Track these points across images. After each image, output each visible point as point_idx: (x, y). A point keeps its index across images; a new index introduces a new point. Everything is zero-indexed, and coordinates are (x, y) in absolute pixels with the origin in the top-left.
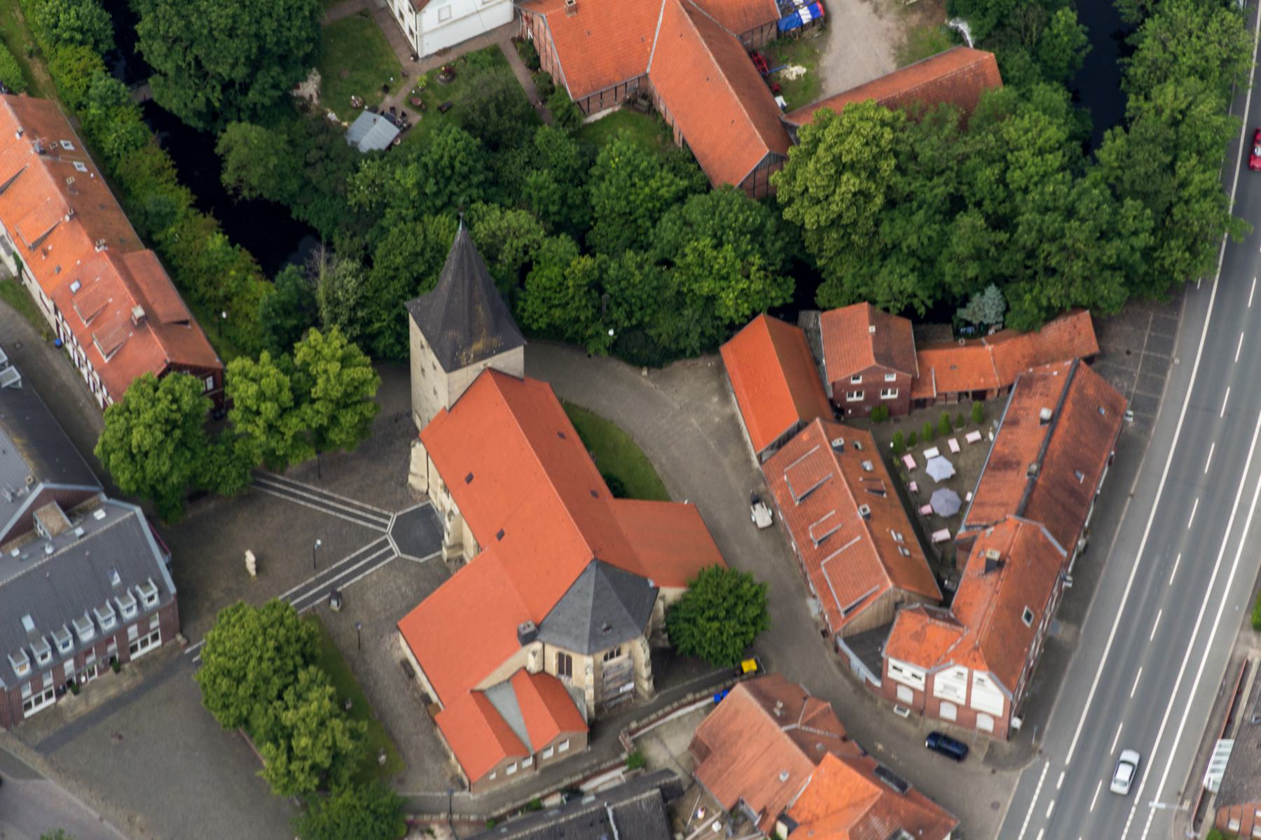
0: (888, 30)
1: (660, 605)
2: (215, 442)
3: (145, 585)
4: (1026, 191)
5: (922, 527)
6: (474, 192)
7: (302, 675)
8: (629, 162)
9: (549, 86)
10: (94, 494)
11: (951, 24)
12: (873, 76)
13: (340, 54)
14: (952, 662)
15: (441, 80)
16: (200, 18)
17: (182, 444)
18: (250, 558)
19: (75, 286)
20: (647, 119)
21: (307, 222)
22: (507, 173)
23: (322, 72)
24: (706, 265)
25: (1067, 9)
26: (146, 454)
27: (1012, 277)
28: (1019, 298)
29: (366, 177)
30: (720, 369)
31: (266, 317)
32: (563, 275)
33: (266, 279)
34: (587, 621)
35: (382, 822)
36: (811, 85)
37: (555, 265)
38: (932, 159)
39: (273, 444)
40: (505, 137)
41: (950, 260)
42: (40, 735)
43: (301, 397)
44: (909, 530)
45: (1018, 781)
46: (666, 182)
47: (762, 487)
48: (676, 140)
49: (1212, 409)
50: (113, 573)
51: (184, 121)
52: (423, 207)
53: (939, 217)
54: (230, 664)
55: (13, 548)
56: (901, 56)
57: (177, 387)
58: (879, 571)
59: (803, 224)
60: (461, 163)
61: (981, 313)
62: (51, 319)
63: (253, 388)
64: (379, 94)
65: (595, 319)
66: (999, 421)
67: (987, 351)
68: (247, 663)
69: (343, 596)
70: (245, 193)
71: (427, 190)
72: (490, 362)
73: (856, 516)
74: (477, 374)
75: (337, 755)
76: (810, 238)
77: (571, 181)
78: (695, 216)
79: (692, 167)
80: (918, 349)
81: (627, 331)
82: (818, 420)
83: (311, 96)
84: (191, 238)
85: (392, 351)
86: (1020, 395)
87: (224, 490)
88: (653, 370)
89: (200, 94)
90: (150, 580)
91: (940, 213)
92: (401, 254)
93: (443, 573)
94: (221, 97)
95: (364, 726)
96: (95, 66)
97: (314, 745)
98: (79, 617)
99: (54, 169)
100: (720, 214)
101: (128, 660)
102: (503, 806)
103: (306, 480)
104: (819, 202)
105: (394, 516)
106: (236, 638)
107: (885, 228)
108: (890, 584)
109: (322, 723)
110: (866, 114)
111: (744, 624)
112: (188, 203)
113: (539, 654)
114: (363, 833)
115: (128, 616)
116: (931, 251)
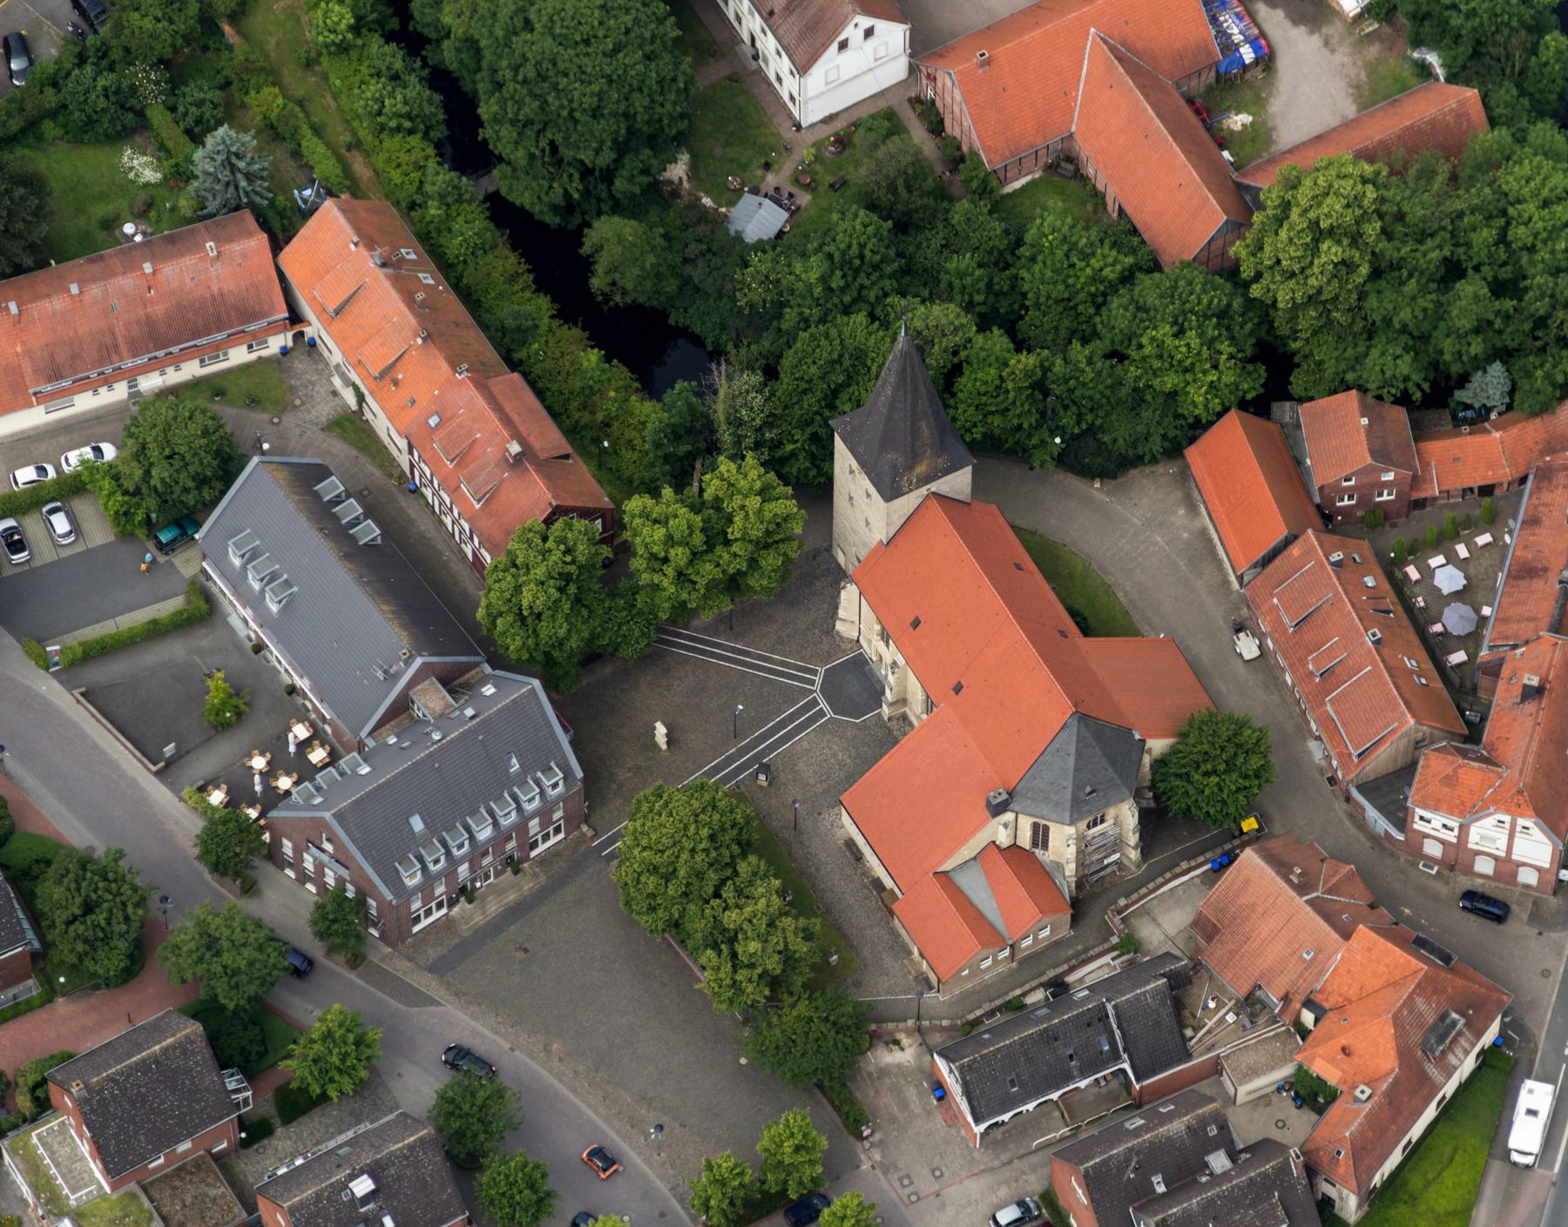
0: (1343, 65)
1: (1147, 760)
2: (613, 595)
3: (547, 770)
4: (1531, 249)
5: (1435, 648)
6: (888, 284)
7: (743, 867)
8: (1064, 240)
9: (958, 153)
10: (477, 665)
11: (1416, 55)
12: (1334, 122)
13: (709, 128)
14: (1492, 810)
15: (830, 152)
16: (558, 97)
17: (578, 601)
18: (661, 730)
19: (433, 421)
20: (1074, 185)
21: (688, 327)
22: (922, 259)
23: (690, 151)
24: (1166, 355)
25: (1556, 33)
26: (539, 616)
27: (1517, 350)
28: (1529, 375)
29: (758, 272)
30: (1185, 475)
31: (657, 445)
32: (1001, 377)
33: (651, 398)
34: (1069, 784)
35: (845, 1035)
36: (1259, 135)
37: (990, 366)
38: (1423, 220)
39: (684, 596)
40: (916, 217)
41: (1448, 336)
42: (432, 954)
43: (716, 537)
44: (1423, 655)
46: (1110, 260)
47: (1245, 612)
48: (1110, 208)
50: (511, 758)
51: (537, 218)
52: (829, 305)
53: (1433, 286)
54: (657, 859)
55: (388, 735)
56: (1360, 96)
57: (569, 535)
59: (1275, 301)
60: (872, 251)
61: (1484, 395)
62: (404, 460)
63: (660, 533)
64: (759, 172)
65: (1038, 426)
66: (1515, 519)
67: (1496, 438)
68: (678, 857)
69: (773, 768)
70: (618, 298)
71: (834, 285)
72: (934, 487)
73: (1364, 643)
74: (920, 500)
75: (789, 959)
76: (1280, 320)
77: (996, 264)
78: (1151, 300)
79: (1136, 240)
80: (1416, 441)
81: (1075, 437)
82: (1310, 531)
83: (680, 179)
84: (558, 355)
85: (807, 475)
86: (1538, 488)
87: (626, 652)
88: (1106, 480)
89: (555, 185)
90: (552, 764)
91: (1433, 281)
92: (814, 363)
93: (888, 736)
94: (581, 187)
95: (816, 924)
96: (427, 158)
97: (763, 950)
98: (474, 812)
99: (397, 281)
100: (1180, 296)
101: (527, 859)
102: (980, 1007)
103: (716, 634)
104: (1293, 275)
105: (822, 671)
106: (663, 828)
107: (1372, 302)
108: (1412, 721)
109: (771, 924)
110: (1343, 170)
111: (1246, 777)
112: (549, 313)
113: (1012, 826)
114: (824, 1049)
115: (529, 808)
116: (1426, 326)
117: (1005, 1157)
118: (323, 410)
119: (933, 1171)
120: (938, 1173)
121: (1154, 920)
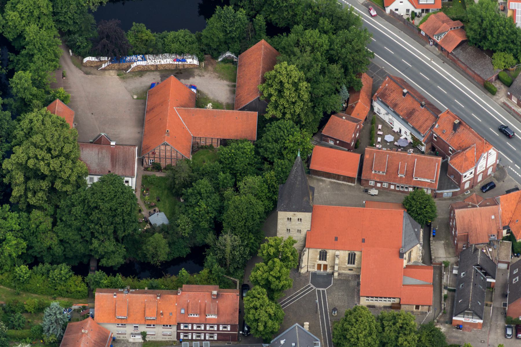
45: (511, 177)
49: (408, 67)
58: (432, 160)
64: (140, 214)
73: (408, 156)
105: (310, 284)
117: (489, 325)
119: (481, 342)
120: (483, 342)
121: (438, 258)
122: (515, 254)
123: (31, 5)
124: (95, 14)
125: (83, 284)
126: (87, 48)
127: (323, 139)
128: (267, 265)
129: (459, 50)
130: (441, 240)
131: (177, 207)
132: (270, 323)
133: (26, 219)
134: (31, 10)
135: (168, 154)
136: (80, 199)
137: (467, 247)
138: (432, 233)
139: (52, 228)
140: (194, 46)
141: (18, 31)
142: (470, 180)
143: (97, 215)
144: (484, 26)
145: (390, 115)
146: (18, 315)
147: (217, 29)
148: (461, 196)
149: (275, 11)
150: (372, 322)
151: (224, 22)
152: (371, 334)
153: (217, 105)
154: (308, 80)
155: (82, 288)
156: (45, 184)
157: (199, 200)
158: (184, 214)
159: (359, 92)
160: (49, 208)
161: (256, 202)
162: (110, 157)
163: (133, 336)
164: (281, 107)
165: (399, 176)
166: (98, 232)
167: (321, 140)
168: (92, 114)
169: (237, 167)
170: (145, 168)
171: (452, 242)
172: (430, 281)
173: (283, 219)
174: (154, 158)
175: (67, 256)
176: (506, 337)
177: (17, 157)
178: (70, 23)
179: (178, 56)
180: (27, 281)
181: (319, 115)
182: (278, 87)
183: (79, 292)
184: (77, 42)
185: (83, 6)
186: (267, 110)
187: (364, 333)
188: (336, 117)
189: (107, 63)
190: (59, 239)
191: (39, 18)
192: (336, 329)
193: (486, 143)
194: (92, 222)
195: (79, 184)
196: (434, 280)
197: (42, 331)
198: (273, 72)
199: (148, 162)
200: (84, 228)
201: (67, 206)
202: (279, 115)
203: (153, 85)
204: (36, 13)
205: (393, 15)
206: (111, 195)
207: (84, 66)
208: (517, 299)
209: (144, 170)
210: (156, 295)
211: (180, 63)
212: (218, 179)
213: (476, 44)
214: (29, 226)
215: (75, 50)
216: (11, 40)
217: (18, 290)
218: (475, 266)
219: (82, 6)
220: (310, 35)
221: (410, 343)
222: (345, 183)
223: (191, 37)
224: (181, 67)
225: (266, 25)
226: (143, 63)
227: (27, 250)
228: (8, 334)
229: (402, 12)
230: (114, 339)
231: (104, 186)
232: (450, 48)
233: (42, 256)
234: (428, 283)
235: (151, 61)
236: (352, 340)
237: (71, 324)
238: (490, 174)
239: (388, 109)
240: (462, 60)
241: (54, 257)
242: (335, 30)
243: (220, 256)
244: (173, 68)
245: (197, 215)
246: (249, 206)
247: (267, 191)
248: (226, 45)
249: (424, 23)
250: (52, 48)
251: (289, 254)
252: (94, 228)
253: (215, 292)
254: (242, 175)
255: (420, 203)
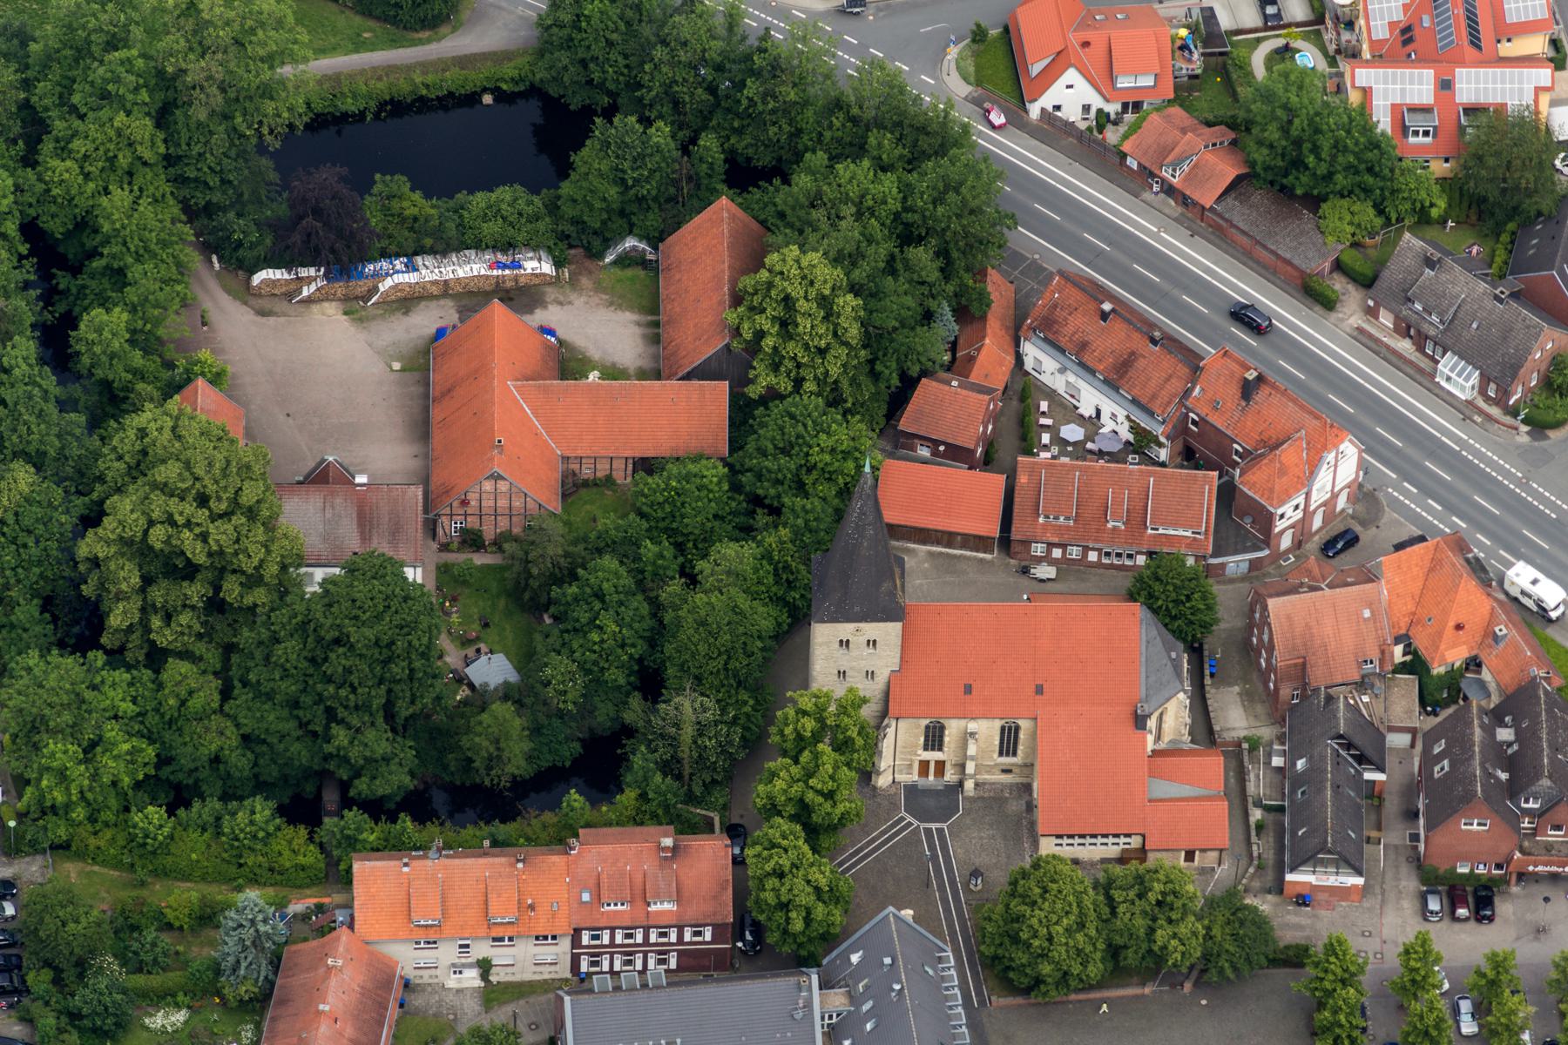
49: (1100, 253)
73: (1131, 472)
105: (904, 813)
117: (1378, 890)
118: (471, 1006)
119: (1363, 935)
122: (1429, 709)
123: (111, 140)
124: (274, 155)
125: (312, 847)
126: (260, 248)
127: (900, 443)
128: (796, 762)
129: (1230, 200)
130: (1231, 685)
131: (538, 637)
132: (820, 911)
133: (150, 685)
134: (111, 154)
135: (503, 503)
136: (294, 621)
137: (1304, 697)
138: (1206, 666)
139: (221, 706)
140: (541, 226)
141: (77, 211)
142: (1292, 526)
143: (343, 662)
144: (1294, 133)
145: (1069, 372)
146: (150, 935)
147: (601, 176)
148: (1271, 570)
149: (743, 126)
150: (1085, 892)
151: (617, 157)
152: (1084, 926)
153: (613, 373)
154: (855, 289)
155: (310, 856)
156: (195, 591)
157: (598, 613)
158: (559, 653)
159: (983, 318)
160: (210, 655)
161: (751, 608)
162: (354, 515)
163: (455, 972)
164: (790, 365)
165: (1110, 525)
166: (346, 707)
167: (896, 447)
168: (288, 415)
169: (687, 525)
170: (442, 545)
171: (1261, 687)
172: (1218, 786)
173: (828, 644)
174: (466, 515)
175: (261, 779)
176: (1426, 919)
177: (120, 522)
178: (211, 184)
179: (499, 256)
180: (165, 848)
181: (888, 380)
182: (780, 312)
183: (303, 869)
184: (234, 231)
185: (244, 136)
186: (752, 374)
187: (1065, 921)
188: (934, 384)
189: (314, 284)
190: (241, 732)
191: (130, 174)
192: (990, 919)
193: (1332, 426)
194: (329, 680)
195: (284, 589)
196: (1226, 786)
197: (218, 972)
198: (764, 275)
199: (450, 527)
200: (307, 700)
201: (261, 643)
202: (785, 385)
203: (440, 333)
204: (124, 161)
205: (1049, 124)
206: (375, 606)
207: (255, 295)
208: (1451, 815)
209: (440, 550)
210: (513, 860)
211: (507, 272)
212: (640, 559)
213: (1272, 183)
214: (160, 704)
215: (227, 253)
216: (59, 236)
217: (141, 873)
218: (1332, 739)
219: (242, 136)
220: (848, 175)
221: (1186, 942)
222: (968, 553)
223: (530, 203)
224: (509, 284)
225: (726, 161)
226: (411, 278)
227: (158, 767)
228: (129, 985)
229: (1072, 113)
230: (407, 985)
231: (356, 583)
232: (1208, 200)
233: (197, 781)
234: (1212, 792)
235: (430, 271)
236: (1036, 943)
237: (294, 948)
238: (1343, 510)
239: (1062, 358)
240: (1241, 225)
241: (229, 783)
242: (909, 162)
243: (663, 752)
244: (488, 288)
245: (595, 652)
246: (736, 618)
247: (771, 579)
248: (625, 218)
249: (1134, 136)
250: (171, 251)
251: (853, 732)
252: (335, 697)
253: (668, 842)
254: (700, 546)
255: (1176, 587)
